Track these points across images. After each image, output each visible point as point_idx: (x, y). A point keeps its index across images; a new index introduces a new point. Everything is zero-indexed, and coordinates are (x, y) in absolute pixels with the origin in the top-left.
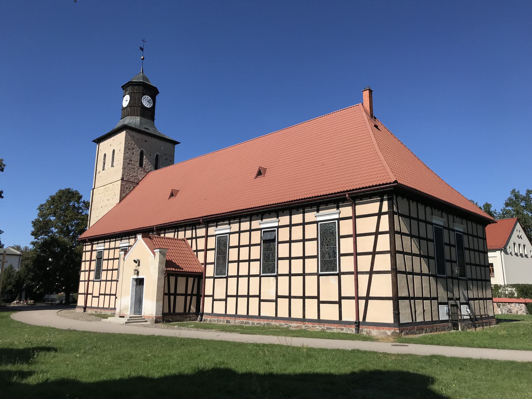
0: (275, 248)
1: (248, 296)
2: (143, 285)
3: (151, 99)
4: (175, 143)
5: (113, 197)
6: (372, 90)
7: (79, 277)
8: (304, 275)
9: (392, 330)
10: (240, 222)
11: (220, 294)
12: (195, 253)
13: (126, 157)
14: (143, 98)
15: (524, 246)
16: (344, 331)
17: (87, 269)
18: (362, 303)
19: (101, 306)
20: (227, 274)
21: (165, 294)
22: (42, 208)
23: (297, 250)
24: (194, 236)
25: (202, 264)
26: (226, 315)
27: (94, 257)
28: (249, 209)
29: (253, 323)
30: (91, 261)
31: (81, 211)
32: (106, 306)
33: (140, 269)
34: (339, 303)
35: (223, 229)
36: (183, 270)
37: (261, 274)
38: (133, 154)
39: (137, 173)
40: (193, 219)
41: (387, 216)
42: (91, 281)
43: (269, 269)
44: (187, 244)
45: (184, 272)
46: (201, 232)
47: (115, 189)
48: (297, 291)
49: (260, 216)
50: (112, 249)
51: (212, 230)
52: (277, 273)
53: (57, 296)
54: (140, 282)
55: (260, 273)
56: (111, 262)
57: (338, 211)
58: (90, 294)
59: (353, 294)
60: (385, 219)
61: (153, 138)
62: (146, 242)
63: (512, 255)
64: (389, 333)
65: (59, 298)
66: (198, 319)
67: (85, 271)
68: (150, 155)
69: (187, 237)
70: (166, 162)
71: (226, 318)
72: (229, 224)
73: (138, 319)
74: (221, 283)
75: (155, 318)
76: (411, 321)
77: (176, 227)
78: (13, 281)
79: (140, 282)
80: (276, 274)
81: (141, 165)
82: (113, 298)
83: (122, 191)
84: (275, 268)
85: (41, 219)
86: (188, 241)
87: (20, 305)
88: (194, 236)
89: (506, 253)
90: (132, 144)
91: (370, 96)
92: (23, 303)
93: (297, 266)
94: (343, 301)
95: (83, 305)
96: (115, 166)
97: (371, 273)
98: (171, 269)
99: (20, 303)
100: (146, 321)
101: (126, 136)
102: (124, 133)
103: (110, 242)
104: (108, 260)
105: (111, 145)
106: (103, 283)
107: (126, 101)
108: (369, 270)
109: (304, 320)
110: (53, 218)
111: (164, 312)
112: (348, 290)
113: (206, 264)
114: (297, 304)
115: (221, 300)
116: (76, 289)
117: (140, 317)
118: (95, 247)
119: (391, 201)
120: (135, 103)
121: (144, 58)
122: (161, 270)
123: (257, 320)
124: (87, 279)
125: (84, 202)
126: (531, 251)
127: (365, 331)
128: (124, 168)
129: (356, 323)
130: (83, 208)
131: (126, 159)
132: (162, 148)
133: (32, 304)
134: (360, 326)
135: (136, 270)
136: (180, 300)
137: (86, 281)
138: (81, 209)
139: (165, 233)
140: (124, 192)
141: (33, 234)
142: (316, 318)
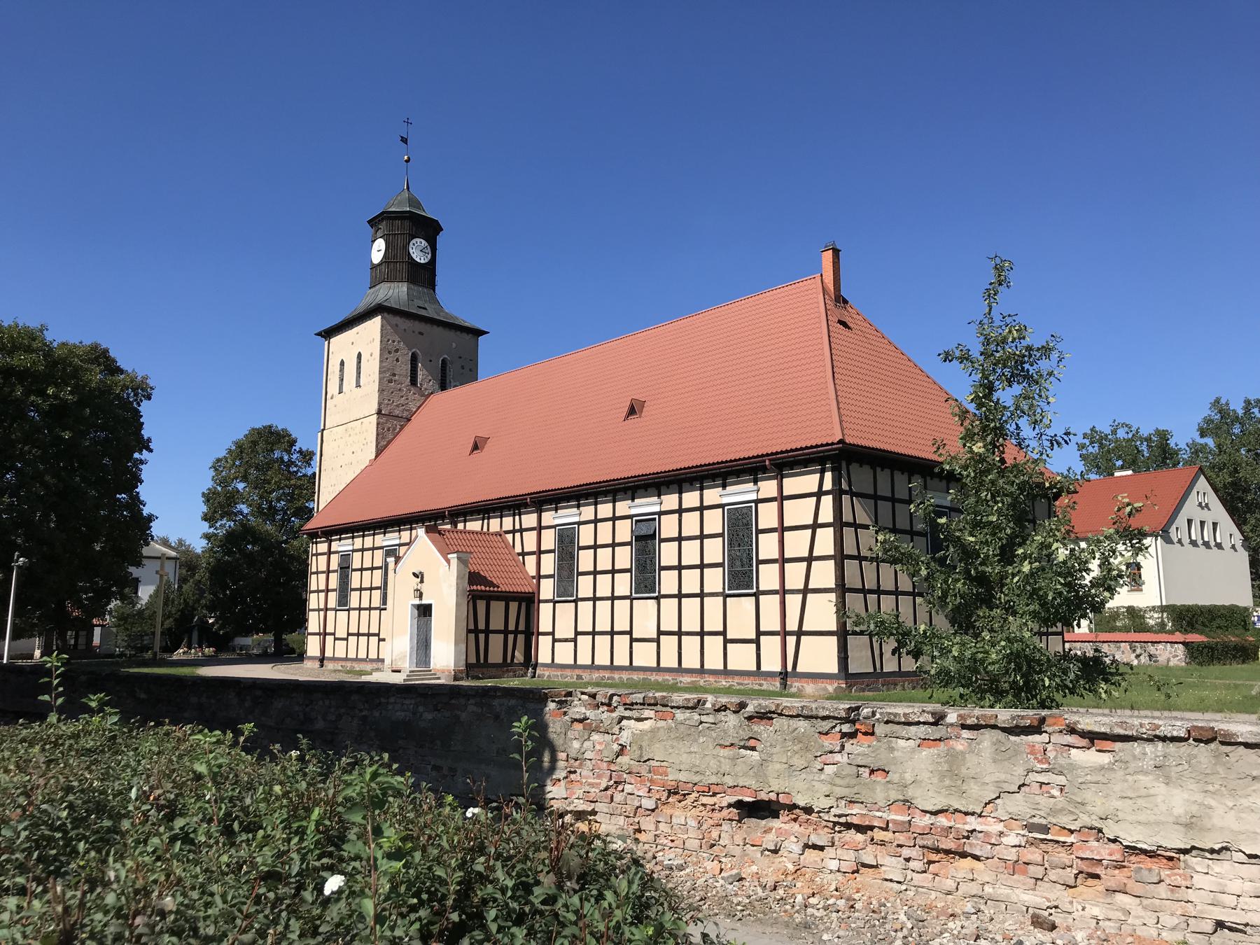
0: (655, 550)
1: (612, 633)
2: (430, 616)
3: (426, 244)
4: (480, 333)
5: (362, 447)
6: (838, 248)
7: (304, 602)
8: (702, 595)
9: (836, 685)
10: (596, 504)
11: (565, 630)
12: (521, 557)
13: (384, 367)
14: (411, 244)
15: (1215, 525)
16: (764, 687)
17: (322, 587)
18: (791, 640)
19: (352, 655)
20: (577, 596)
21: (469, 631)
22: (220, 466)
23: (691, 553)
24: (517, 527)
25: (533, 577)
26: (575, 666)
27: (334, 566)
28: (610, 481)
29: (621, 678)
30: (328, 572)
31: (295, 469)
32: (362, 655)
33: (424, 588)
34: (757, 642)
35: (567, 515)
36: (499, 589)
37: (633, 595)
38: (397, 360)
39: (407, 399)
40: (514, 496)
41: (830, 497)
42: (332, 609)
43: (646, 586)
44: (505, 541)
45: (501, 592)
46: (529, 520)
47: (367, 431)
48: (691, 624)
49: (630, 493)
50: (368, 549)
51: (548, 518)
52: (659, 592)
53: (253, 641)
54: (424, 611)
55: (631, 593)
56: (367, 574)
57: (755, 488)
58: (330, 634)
59: (777, 628)
60: (827, 501)
61: (435, 327)
62: (433, 542)
63: (1182, 545)
64: (831, 688)
65: (259, 644)
66: (529, 675)
67: (318, 591)
68: (431, 361)
69: (505, 529)
70: (462, 374)
71: (577, 670)
72: (578, 506)
73: (424, 675)
74: (565, 610)
75: (453, 673)
76: (872, 670)
77: (485, 510)
78: (174, 611)
79: (424, 611)
80: (657, 594)
81: (414, 381)
82: (374, 640)
83: (381, 436)
84: (655, 584)
85: (219, 489)
86: (507, 536)
87: (191, 657)
88: (517, 527)
89: (1168, 540)
90: (394, 341)
91: (836, 260)
92: (195, 654)
93: (691, 581)
94: (762, 638)
95: (318, 654)
96: (365, 385)
97: (805, 591)
98: (479, 587)
99: (190, 653)
100: (439, 678)
101: (382, 326)
102: (377, 322)
103: (363, 536)
104: (362, 570)
105: (353, 343)
106: (354, 614)
107: (378, 252)
108: (802, 587)
109: (702, 671)
110: (241, 486)
111: (469, 662)
112: (771, 621)
113: (539, 577)
114: (691, 644)
115: (566, 640)
116: (300, 621)
117: (427, 671)
118: (335, 546)
119: (837, 473)
120: (395, 256)
121: (409, 158)
122: (460, 588)
123: (627, 673)
124: (322, 606)
125: (300, 452)
126: (1231, 535)
127: (795, 685)
128: (381, 391)
129: (781, 673)
130: (300, 464)
131: (384, 372)
132: (454, 345)
133: (212, 656)
134: (788, 679)
135: (417, 590)
136: (496, 641)
137: (322, 610)
138: (296, 466)
139: (465, 521)
140: (383, 438)
141: (205, 518)
142: (721, 667)
